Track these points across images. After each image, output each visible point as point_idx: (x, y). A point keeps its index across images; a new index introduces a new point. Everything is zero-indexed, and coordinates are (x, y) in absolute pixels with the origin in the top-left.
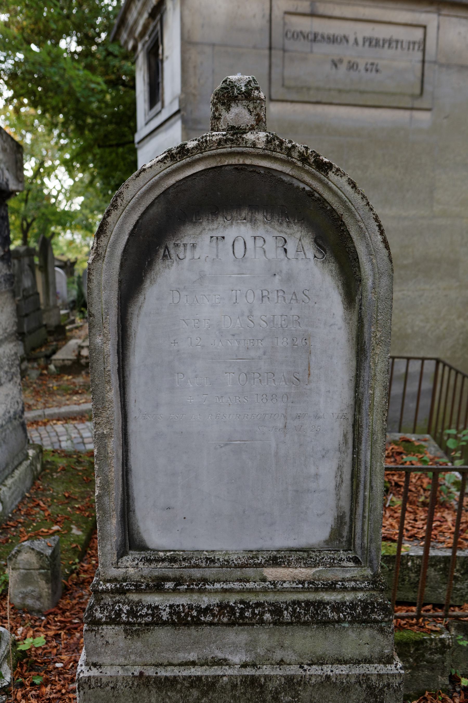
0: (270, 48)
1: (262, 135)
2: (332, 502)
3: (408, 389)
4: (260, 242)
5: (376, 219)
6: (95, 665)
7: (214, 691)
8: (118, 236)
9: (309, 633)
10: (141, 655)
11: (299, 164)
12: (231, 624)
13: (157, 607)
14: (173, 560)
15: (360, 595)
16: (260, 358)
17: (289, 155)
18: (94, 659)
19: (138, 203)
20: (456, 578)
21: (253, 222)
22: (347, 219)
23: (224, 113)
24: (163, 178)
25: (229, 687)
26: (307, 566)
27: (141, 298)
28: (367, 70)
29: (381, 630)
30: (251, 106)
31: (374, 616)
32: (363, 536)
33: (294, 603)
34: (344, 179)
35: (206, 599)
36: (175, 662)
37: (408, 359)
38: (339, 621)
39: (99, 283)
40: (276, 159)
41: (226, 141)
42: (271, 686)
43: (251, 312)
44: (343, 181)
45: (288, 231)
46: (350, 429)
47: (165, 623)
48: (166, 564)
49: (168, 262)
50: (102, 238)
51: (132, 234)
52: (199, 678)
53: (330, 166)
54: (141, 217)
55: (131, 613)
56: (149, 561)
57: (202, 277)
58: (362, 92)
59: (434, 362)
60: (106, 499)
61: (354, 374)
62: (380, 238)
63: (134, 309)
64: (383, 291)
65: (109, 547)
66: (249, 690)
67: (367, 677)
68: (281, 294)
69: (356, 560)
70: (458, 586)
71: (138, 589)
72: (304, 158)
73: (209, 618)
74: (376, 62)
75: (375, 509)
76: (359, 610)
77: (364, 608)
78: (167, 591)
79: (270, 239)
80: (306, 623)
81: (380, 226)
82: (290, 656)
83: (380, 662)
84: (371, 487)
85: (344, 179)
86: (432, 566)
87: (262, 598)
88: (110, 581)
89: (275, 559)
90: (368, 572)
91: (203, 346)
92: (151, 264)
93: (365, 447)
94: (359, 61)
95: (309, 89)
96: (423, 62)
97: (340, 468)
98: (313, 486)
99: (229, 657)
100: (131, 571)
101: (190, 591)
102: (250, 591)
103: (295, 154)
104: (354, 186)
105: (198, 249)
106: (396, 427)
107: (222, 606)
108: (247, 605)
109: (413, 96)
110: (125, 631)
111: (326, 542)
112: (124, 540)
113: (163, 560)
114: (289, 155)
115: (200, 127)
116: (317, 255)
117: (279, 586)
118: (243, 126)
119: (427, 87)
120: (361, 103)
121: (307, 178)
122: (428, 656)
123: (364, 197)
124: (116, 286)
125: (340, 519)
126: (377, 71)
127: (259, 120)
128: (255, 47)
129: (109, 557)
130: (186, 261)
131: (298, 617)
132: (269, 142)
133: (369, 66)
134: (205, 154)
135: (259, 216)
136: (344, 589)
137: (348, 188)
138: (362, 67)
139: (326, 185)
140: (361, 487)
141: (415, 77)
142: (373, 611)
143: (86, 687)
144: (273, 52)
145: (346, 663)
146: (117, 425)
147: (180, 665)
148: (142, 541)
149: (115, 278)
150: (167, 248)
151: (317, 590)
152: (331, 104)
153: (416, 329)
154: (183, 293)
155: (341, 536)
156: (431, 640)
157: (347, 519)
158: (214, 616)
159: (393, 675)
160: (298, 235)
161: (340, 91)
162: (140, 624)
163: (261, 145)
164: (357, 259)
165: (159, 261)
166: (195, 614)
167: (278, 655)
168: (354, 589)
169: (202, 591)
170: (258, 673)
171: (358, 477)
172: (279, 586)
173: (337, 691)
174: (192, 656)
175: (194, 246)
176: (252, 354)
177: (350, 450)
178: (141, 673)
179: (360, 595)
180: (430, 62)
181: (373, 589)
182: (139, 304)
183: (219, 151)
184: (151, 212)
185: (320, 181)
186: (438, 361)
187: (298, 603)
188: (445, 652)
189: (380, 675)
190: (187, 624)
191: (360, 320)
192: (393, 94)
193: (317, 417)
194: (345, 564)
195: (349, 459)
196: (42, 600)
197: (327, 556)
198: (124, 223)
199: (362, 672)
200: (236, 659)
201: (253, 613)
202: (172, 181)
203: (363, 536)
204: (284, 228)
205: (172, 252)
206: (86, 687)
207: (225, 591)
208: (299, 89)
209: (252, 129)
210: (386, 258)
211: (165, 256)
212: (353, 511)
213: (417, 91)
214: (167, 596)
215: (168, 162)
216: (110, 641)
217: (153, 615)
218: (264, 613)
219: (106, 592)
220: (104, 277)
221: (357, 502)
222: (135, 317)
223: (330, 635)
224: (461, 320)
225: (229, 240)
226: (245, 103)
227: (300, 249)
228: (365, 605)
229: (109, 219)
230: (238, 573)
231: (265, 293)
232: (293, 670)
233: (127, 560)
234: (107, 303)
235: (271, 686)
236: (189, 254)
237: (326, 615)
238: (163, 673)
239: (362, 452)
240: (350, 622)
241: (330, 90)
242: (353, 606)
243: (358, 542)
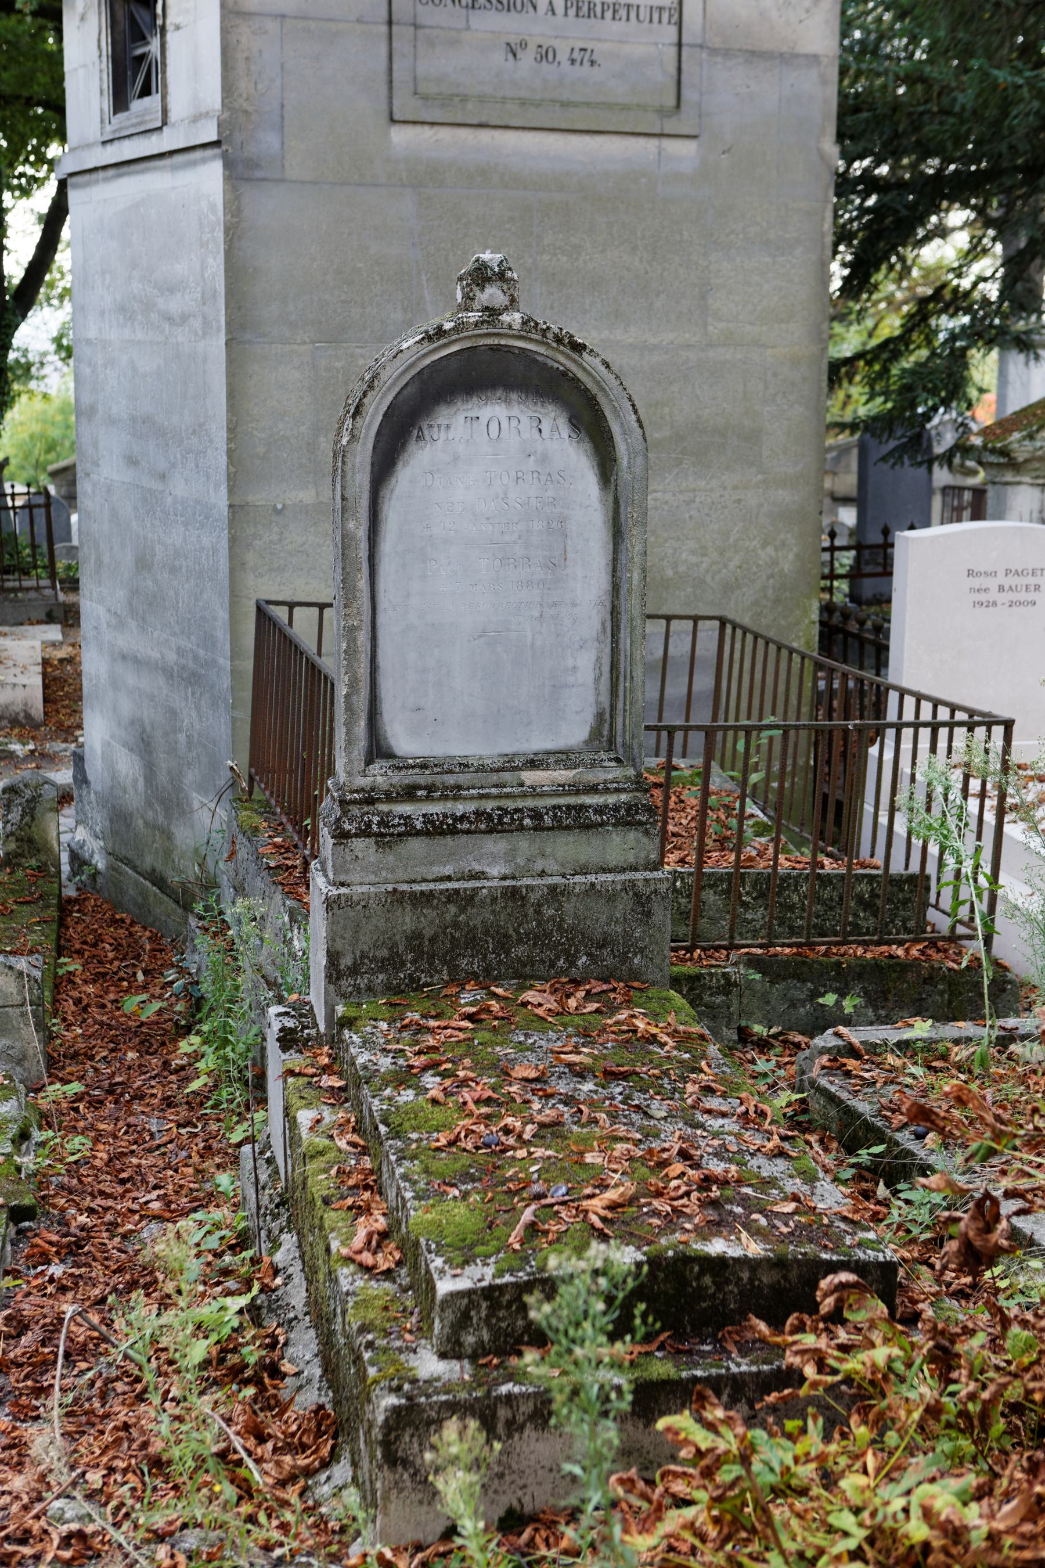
0: (390, 23)
1: (517, 316)
2: (591, 698)
3: (668, 691)
4: (514, 422)
5: (630, 399)
6: (342, 884)
7: (473, 907)
8: (373, 417)
9: (571, 839)
10: (393, 871)
11: (554, 345)
12: (490, 831)
13: (409, 817)
14: (424, 766)
15: (624, 797)
16: (515, 542)
17: (544, 336)
18: (342, 878)
19: (394, 384)
20: (745, 905)
21: (508, 402)
22: (601, 399)
23: (478, 293)
24: (419, 359)
25: (488, 900)
26: (567, 768)
27: (393, 481)
28: (573, 61)
29: (647, 833)
30: (505, 287)
31: (638, 817)
32: (624, 732)
33: (554, 807)
34: (598, 360)
35: (461, 807)
36: (430, 877)
37: (669, 618)
38: (602, 824)
39: (353, 466)
40: (531, 340)
41: (482, 322)
42: (533, 897)
43: (505, 494)
44: (597, 362)
45: (543, 411)
46: (608, 617)
47: (418, 833)
48: (417, 770)
49: (422, 443)
50: (358, 419)
51: (385, 415)
52: (457, 891)
53: (583, 347)
54: (395, 398)
55: (381, 823)
56: (399, 768)
57: (456, 458)
58: (565, 105)
59: (717, 623)
60: (355, 698)
61: (611, 557)
62: (634, 417)
63: (385, 493)
64: (638, 471)
65: (356, 753)
66: (510, 903)
67: (633, 883)
68: (536, 475)
69: (618, 760)
70: (749, 916)
71: (389, 798)
72: (558, 340)
73: (465, 826)
74: (589, 46)
75: (637, 701)
76: (622, 812)
77: (628, 810)
78: (419, 800)
79: (524, 419)
80: (568, 828)
81: (633, 406)
82: (552, 866)
83: (646, 869)
84: (632, 678)
85: (598, 360)
86: (711, 886)
87: (520, 804)
88: (356, 791)
89: (532, 761)
90: (631, 772)
91: (456, 531)
92: (404, 445)
93: (624, 635)
94: (556, 43)
95: (464, 99)
96: (680, 45)
97: (598, 659)
98: (571, 680)
99: (487, 869)
100: (380, 779)
101: (444, 798)
102: (508, 796)
103: (550, 335)
104: (608, 367)
105: (452, 429)
106: (653, 753)
107: (478, 814)
108: (505, 811)
109: (662, 112)
110: (377, 843)
111: (586, 742)
112: (370, 746)
113: (413, 767)
114: (544, 336)
115: (259, 174)
116: (573, 435)
117: (538, 790)
118: (497, 306)
119: (687, 93)
120: (563, 126)
121: (561, 359)
122: (706, 998)
123: (617, 377)
124: (368, 468)
125: (600, 716)
126: (592, 63)
127: (513, 300)
128: (359, 21)
129: (356, 763)
130: (440, 443)
131: (560, 821)
132: (524, 323)
133: (576, 55)
134: (462, 335)
135: (514, 396)
136: (607, 791)
137: (602, 368)
138: (563, 57)
139: (580, 366)
140: (622, 679)
141: (662, 75)
142: (637, 813)
143: (335, 906)
144: (395, 28)
145: (610, 871)
146: (367, 617)
147: (435, 880)
148: (389, 747)
149: (368, 460)
150: (420, 429)
151: (578, 792)
152: (507, 127)
153: (682, 569)
154: (436, 476)
155: (601, 735)
156: (711, 975)
157: (607, 716)
158: (471, 823)
159: (660, 880)
160: (553, 415)
161: (523, 103)
162: (392, 835)
163: (517, 325)
164: (611, 438)
165: (413, 442)
166: (450, 821)
167: (539, 865)
168: (617, 790)
169: (456, 798)
170: (519, 883)
171: (617, 669)
172: (538, 790)
173: (603, 901)
174: (448, 870)
175: (448, 427)
176: (507, 538)
177: (609, 640)
178: (395, 890)
179: (624, 797)
180: (690, 46)
181: (637, 790)
182: (391, 487)
183: (476, 332)
184: (405, 392)
185: (575, 361)
186: (723, 622)
187: (560, 807)
188: (730, 992)
189: (646, 880)
190: (443, 833)
191: (616, 502)
192: (626, 108)
193: (574, 605)
194: (606, 764)
195: (608, 650)
196: (26, 1064)
197: (587, 757)
198: (379, 404)
199: (628, 877)
200: (495, 871)
201: (512, 819)
202: (427, 361)
203: (624, 732)
204: (539, 408)
205: (426, 432)
206: (335, 906)
207: (482, 797)
208: (446, 100)
209: (506, 309)
210: (640, 437)
211: (418, 437)
212: (613, 707)
213: (671, 101)
214: (419, 805)
215: (426, 343)
216: (360, 855)
217: (405, 825)
218: (523, 818)
219: (354, 802)
220: (358, 460)
221: (617, 696)
222: (386, 500)
223: (593, 840)
224: (770, 550)
225: (484, 421)
226: (499, 283)
227: (555, 429)
228: (629, 807)
229: (365, 401)
230: (494, 778)
231: (520, 474)
232: (557, 880)
233: (375, 768)
234: (360, 486)
235: (533, 897)
236: (443, 434)
237: (588, 818)
238: (417, 888)
239: (622, 641)
240: (614, 825)
241: (504, 100)
242: (616, 808)
243: (619, 740)
